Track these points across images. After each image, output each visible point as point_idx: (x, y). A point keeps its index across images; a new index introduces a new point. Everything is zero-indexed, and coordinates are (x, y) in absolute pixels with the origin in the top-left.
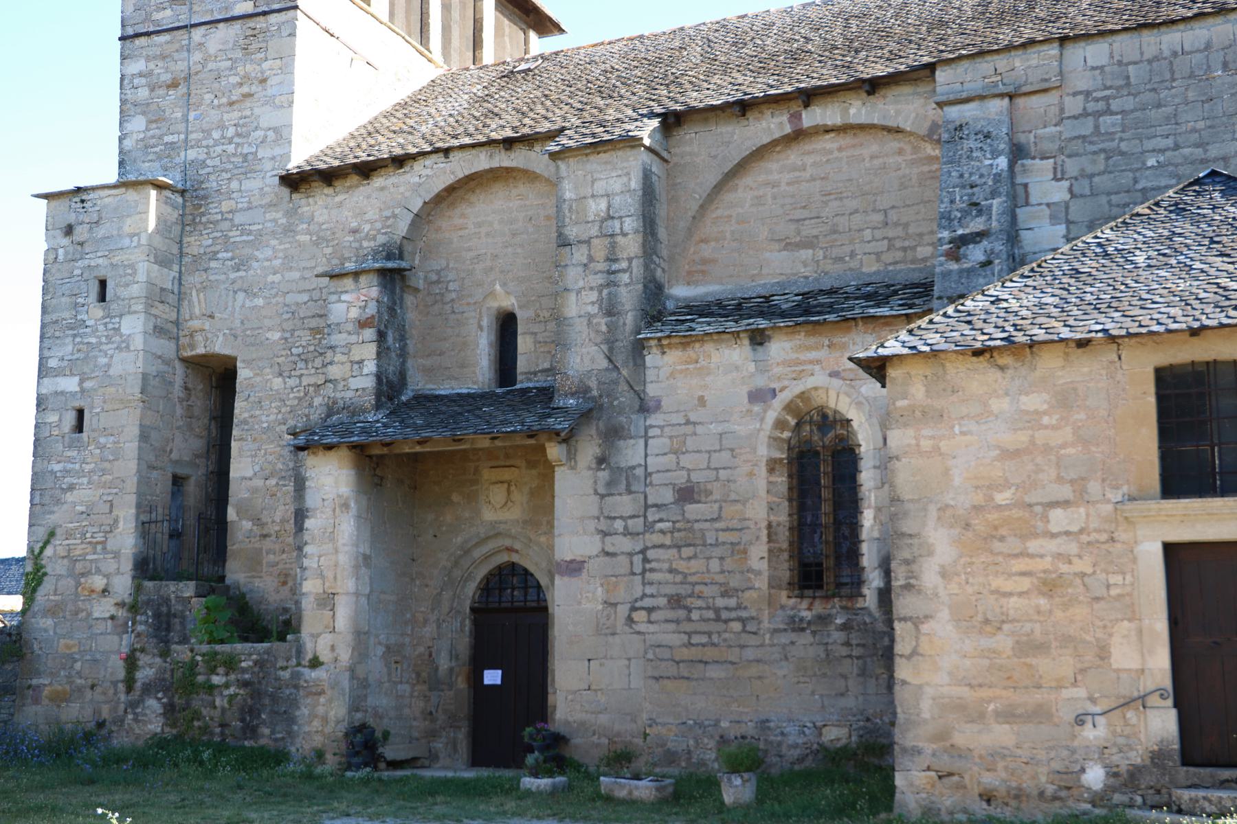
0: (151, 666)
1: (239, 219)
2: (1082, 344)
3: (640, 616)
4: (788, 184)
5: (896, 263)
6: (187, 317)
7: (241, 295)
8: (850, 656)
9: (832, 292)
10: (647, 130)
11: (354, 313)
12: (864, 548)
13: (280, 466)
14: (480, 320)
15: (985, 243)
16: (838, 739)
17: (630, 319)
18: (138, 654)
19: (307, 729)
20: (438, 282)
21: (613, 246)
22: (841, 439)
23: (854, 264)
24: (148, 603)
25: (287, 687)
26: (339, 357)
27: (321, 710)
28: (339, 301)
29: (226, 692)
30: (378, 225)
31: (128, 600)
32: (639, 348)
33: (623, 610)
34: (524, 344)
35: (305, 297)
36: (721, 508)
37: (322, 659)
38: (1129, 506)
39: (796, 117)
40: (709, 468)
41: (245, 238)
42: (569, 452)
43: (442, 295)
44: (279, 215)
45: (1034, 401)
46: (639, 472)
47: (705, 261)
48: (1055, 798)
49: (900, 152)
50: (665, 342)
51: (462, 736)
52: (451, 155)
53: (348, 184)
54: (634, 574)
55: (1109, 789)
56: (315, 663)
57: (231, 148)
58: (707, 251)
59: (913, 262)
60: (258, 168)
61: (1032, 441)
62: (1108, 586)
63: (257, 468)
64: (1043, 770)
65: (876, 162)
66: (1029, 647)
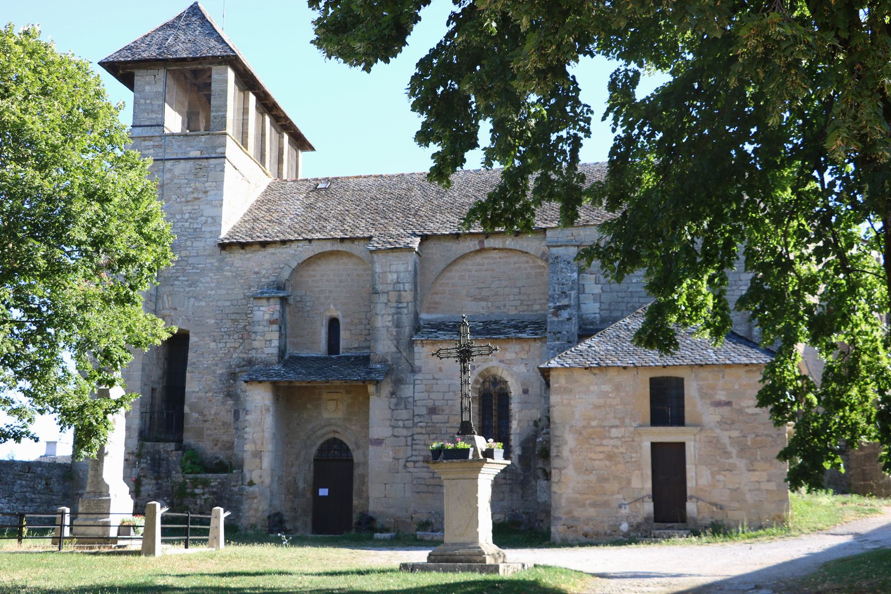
0: (149, 484)
1: (191, 261)
2: (625, 368)
3: (410, 465)
4: (476, 271)
5: (524, 311)
6: (161, 308)
7: (192, 300)
8: (506, 484)
9: (496, 322)
10: (416, 243)
11: (267, 317)
12: (512, 437)
13: (214, 387)
14: (322, 321)
15: (568, 310)
16: (500, 519)
17: (407, 330)
18: (142, 478)
19: (247, 515)
20: (301, 301)
21: (400, 296)
22: (501, 389)
23: (505, 310)
24: (148, 453)
25: (236, 495)
26: (259, 338)
27: (255, 506)
28: (259, 310)
29: (203, 497)
30: (270, 271)
31: (136, 451)
32: (411, 344)
33: (402, 462)
34: (344, 335)
35: (229, 303)
36: (448, 418)
37: (254, 482)
38: (640, 428)
39: (482, 242)
40: (443, 399)
41: (194, 271)
42: (377, 389)
43: (303, 308)
44: (215, 261)
45: (606, 388)
46: (411, 400)
47: (436, 303)
48: (610, 535)
49: (527, 262)
50: (424, 342)
51: (309, 519)
52: (313, 242)
53: (253, 249)
54: (407, 446)
55: (629, 531)
56: (251, 484)
57: (187, 224)
58: (437, 298)
59: (531, 311)
60: (203, 236)
61: (605, 403)
62: (631, 458)
63: (201, 387)
64: (606, 525)
65: (517, 266)
66: (603, 479)
